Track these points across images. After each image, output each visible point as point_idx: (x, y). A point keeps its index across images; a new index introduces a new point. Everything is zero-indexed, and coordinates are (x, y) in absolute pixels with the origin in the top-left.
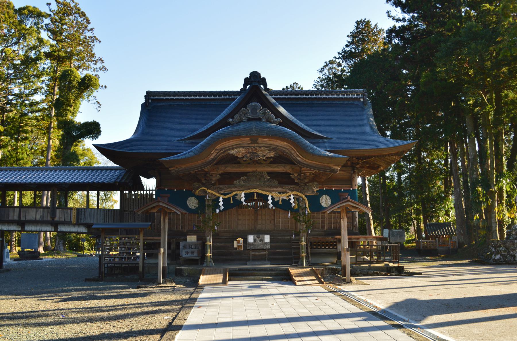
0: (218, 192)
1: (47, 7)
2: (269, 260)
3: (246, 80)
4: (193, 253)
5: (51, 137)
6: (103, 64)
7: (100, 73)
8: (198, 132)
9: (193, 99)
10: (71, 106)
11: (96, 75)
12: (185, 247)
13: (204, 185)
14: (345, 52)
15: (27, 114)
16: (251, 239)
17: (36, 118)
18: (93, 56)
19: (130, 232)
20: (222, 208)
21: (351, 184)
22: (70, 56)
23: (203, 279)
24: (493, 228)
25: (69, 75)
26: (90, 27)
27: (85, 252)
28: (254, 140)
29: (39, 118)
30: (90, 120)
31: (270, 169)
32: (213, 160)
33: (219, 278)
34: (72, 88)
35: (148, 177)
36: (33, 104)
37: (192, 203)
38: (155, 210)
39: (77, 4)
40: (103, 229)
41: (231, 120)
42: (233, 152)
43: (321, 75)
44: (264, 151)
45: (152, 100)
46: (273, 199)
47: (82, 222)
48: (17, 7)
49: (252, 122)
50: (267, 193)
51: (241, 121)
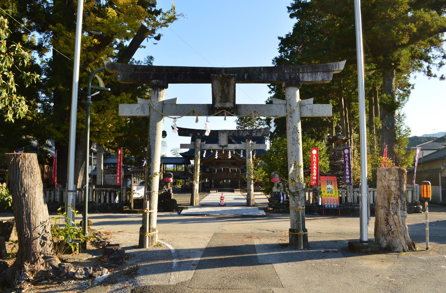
16: (225, 181)
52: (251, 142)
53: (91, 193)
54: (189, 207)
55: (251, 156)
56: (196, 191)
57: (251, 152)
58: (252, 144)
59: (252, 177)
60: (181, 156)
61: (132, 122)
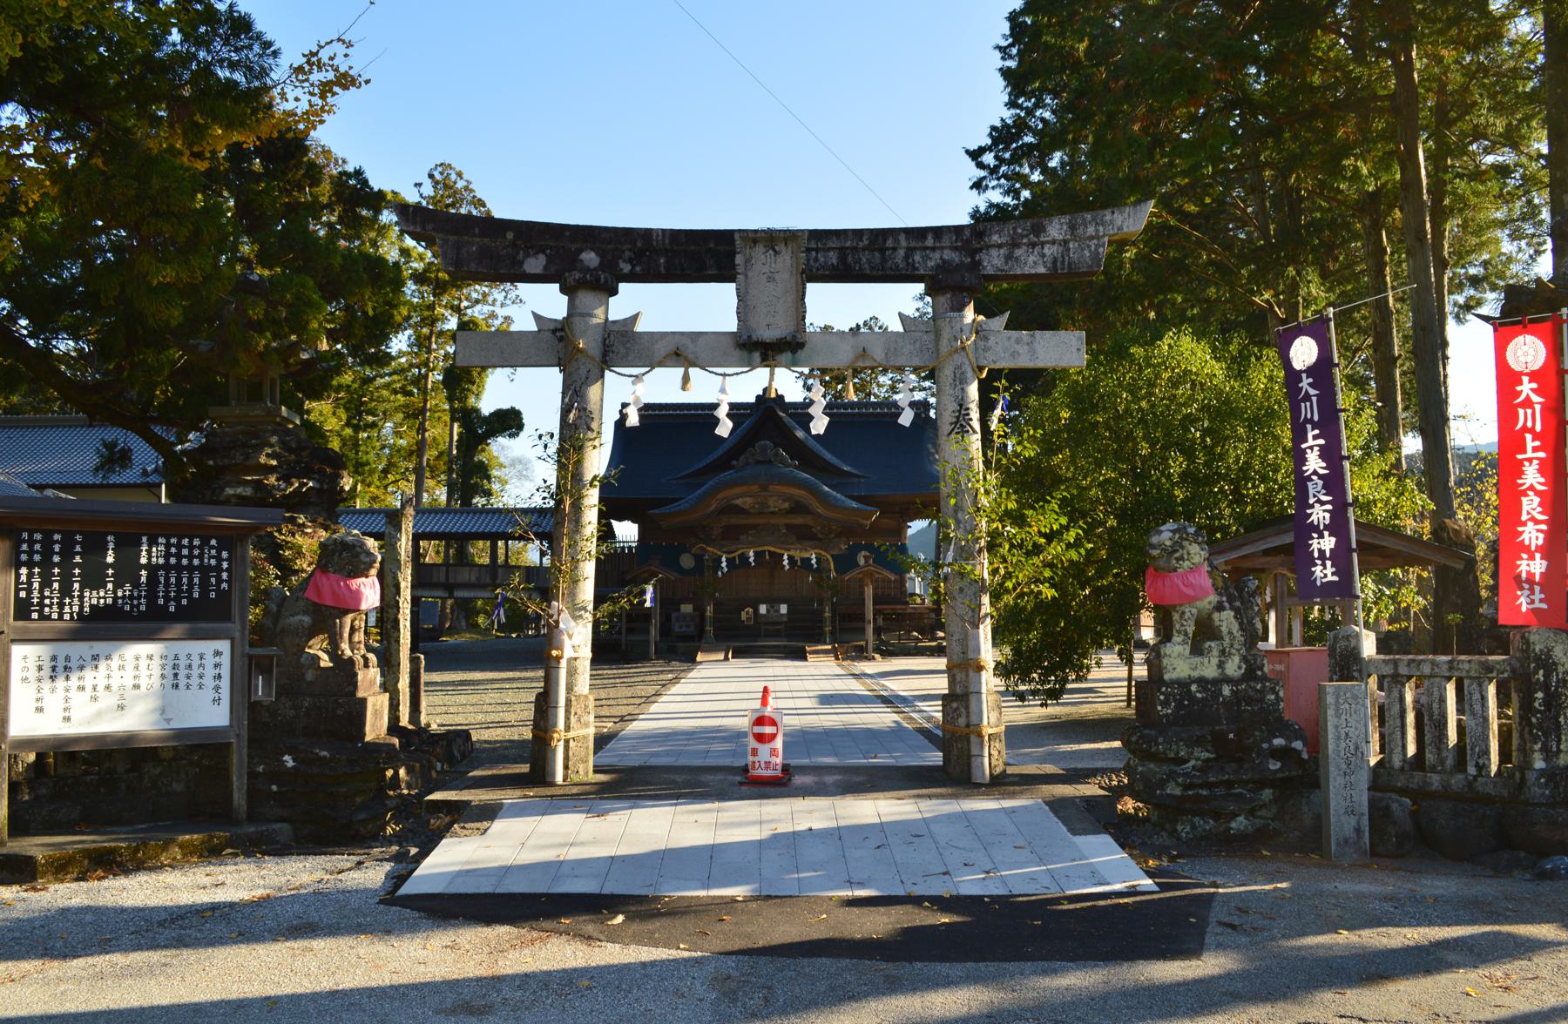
16: (763, 609)
23: (699, 658)
28: (764, 488)
30: (506, 406)
33: (721, 656)
35: (620, 519)
37: (687, 561)
42: (738, 502)
43: (920, 304)
46: (790, 558)
52: (969, 315)
54: (509, 796)
55: (975, 415)
56: (572, 673)
57: (973, 390)
58: (978, 329)
59: (983, 568)
61: (98, 161)
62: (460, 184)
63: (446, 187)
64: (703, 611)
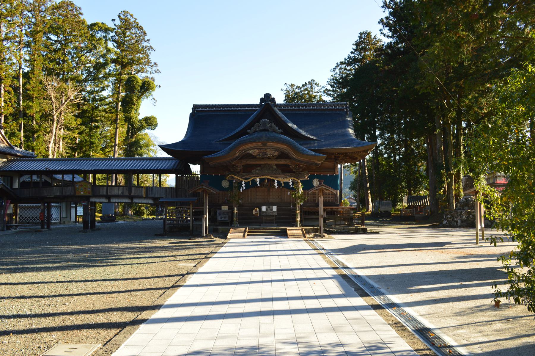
0: (241, 178)
1: (113, 22)
2: (276, 223)
3: (262, 99)
4: (225, 218)
5: (118, 126)
6: (157, 68)
7: (155, 75)
8: (228, 136)
9: (225, 110)
10: (134, 105)
11: (152, 78)
12: (220, 214)
13: (232, 173)
14: (350, 58)
15: (98, 107)
16: (264, 209)
17: (104, 110)
18: (149, 62)
19: (182, 204)
20: (244, 188)
21: (334, 171)
22: (131, 63)
23: (229, 235)
24: (451, 200)
25: (133, 81)
26: (146, 38)
27: (145, 216)
28: (264, 144)
29: (107, 110)
31: (276, 162)
32: (237, 157)
34: (135, 90)
35: (194, 164)
36: (102, 99)
38: (200, 191)
39: (136, 19)
40: (166, 202)
41: (249, 131)
42: (251, 152)
43: (333, 73)
44: (271, 151)
45: (197, 111)
46: (278, 182)
47: (150, 196)
48: (89, 23)
49: (263, 133)
50: (274, 178)
51: (256, 132)
53: (64, 257)
60: (165, 155)
62: (132, 20)
63: (126, 21)
64: (233, 210)
